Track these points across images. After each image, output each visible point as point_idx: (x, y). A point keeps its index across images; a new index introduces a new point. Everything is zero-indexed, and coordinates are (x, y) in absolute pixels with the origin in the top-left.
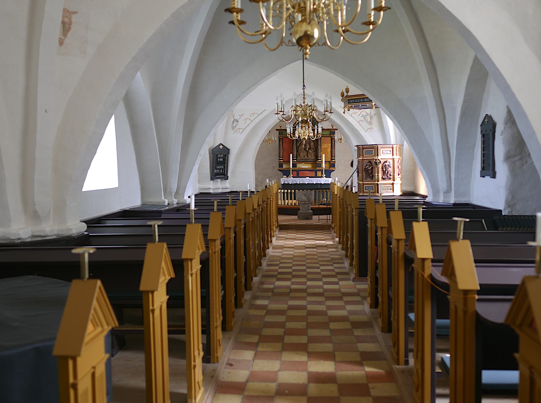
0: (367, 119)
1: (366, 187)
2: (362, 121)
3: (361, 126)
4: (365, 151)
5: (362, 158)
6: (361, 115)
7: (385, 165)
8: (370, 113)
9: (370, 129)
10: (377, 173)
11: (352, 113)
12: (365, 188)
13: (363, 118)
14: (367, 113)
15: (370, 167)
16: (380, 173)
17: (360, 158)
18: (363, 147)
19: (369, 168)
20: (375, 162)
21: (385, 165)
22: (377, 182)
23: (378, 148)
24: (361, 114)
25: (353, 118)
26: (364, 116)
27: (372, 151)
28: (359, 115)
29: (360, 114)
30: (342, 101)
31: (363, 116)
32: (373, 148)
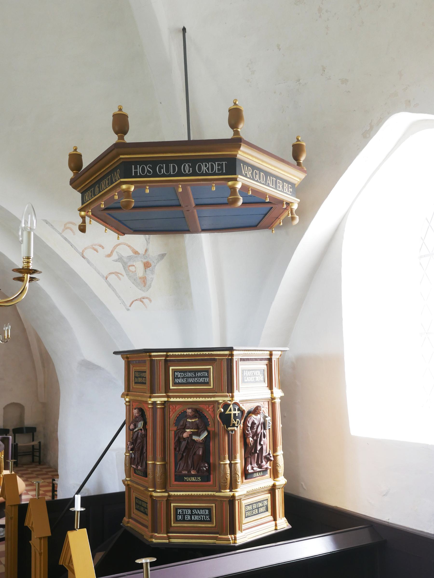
0: (132, 268)
1: (180, 511)
2: (116, 273)
3: (114, 290)
4: (174, 371)
5: (166, 399)
6: (115, 256)
7: (253, 423)
8: (146, 250)
9: (141, 300)
10: (227, 456)
11: (85, 249)
12: (176, 514)
13: (120, 265)
14: (136, 253)
15: (199, 435)
16: (238, 456)
17: (153, 400)
18: (167, 356)
19: (195, 438)
20: (221, 415)
21: (253, 423)
22: (227, 493)
23: (230, 362)
24: (115, 254)
25: (89, 262)
26: (125, 260)
27: (207, 371)
28: (109, 256)
29: (112, 252)
30: (75, 188)
31: (120, 259)
32: (211, 361)
